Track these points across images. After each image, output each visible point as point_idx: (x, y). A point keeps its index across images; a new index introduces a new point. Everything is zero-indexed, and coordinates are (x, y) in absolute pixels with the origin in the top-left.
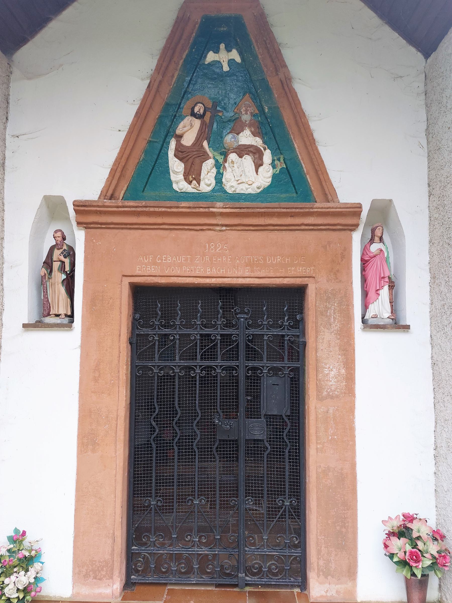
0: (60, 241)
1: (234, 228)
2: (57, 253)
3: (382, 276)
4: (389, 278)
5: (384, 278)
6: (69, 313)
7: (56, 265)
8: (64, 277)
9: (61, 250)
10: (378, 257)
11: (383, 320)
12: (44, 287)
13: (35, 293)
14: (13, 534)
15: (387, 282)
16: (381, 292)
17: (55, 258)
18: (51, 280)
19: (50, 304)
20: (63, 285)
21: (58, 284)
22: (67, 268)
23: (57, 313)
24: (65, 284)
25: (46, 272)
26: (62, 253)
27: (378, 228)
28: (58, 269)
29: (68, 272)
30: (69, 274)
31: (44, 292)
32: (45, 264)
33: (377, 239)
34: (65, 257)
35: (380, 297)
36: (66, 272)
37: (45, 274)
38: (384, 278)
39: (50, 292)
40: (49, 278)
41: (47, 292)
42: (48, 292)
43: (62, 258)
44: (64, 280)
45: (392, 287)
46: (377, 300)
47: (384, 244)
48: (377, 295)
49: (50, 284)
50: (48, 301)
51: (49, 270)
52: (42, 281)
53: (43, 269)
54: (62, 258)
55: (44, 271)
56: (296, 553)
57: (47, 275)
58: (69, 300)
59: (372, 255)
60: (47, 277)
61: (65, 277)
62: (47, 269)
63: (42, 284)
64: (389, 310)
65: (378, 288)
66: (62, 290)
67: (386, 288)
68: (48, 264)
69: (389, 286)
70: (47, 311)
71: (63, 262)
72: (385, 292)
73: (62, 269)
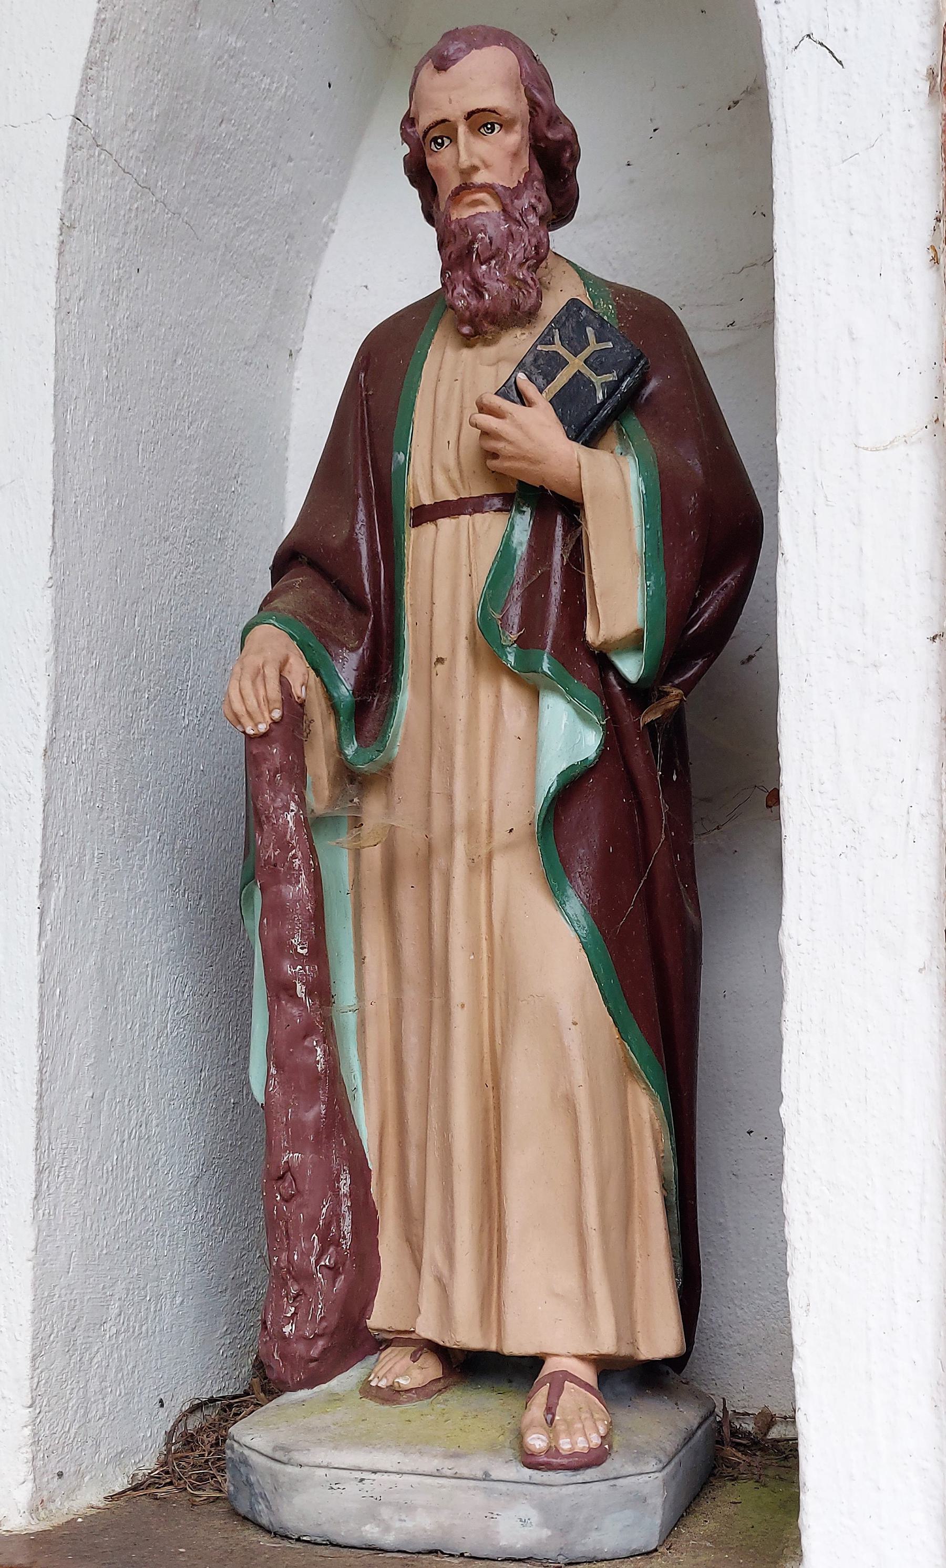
0: (505, 198)
1: (391, 1130)
2: (455, 385)
6: (661, 1339)
7: (451, 569)
8: (568, 735)
9: (518, 343)
12: (275, 910)
13: (156, 982)
17: (431, 462)
18: (374, 809)
19: (361, 1175)
20: (557, 868)
21: (482, 865)
22: (622, 599)
23: (468, 1336)
24: (585, 853)
25: (299, 673)
26: (542, 366)
28: (486, 627)
29: (631, 667)
30: (640, 694)
31: (280, 989)
32: (298, 579)
34: (587, 429)
36: (602, 661)
37: (294, 711)
39: (362, 982)
40: (352, 779)
41: (322, 990)
42: (345, 992)
43: (540, 436)
44: (572, 785)
49: (373, 856)
50: (339, 1121)
51: (347, 670)
52: (256, 817)
53: (273, 641)
54: (540, 436)
55: (267, 669)
57: (322, 729)
58: (646, 1108)
60: (319, 766)
61: (589, 742)
62: (318, 646)
63: (263, 866)
66: (553, 950)
68: (341, 575)
70: (327, 1291)
71: (556, 508)
73: (541, 623)
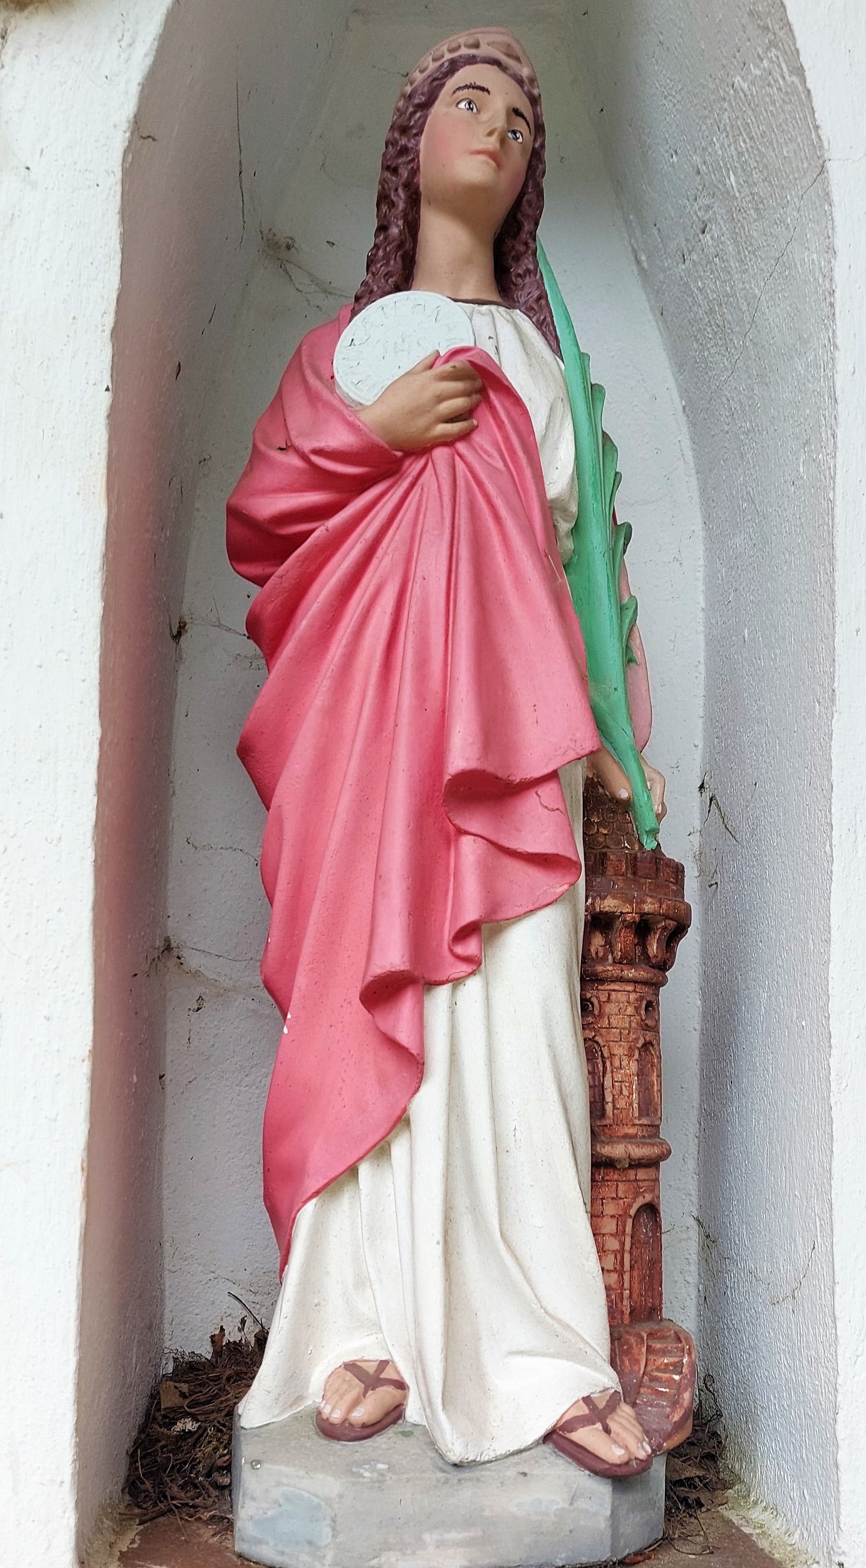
3: (462, 755)
4: (603, 808)
5: (490, 790)
10: (435, 475)
11: (466, 1495)
14: (667, 973)
15: (545, 861)
16: (450, 1017)
27: (464, 75)
33: (444, 238)
35: (428, 1104)
38: (490, 790)
45: (634, 928)
46: (399, 1149)
47: (546, 327)
48: (390, 1063)
56: (615, 1323)
59: (339, 438)
64: (586, 1314)
65: (392, 956)
67: (534, 959)
69: (598, 922)
72: (513, 1012)
